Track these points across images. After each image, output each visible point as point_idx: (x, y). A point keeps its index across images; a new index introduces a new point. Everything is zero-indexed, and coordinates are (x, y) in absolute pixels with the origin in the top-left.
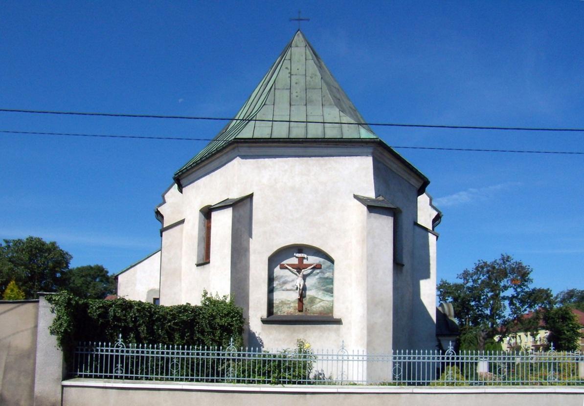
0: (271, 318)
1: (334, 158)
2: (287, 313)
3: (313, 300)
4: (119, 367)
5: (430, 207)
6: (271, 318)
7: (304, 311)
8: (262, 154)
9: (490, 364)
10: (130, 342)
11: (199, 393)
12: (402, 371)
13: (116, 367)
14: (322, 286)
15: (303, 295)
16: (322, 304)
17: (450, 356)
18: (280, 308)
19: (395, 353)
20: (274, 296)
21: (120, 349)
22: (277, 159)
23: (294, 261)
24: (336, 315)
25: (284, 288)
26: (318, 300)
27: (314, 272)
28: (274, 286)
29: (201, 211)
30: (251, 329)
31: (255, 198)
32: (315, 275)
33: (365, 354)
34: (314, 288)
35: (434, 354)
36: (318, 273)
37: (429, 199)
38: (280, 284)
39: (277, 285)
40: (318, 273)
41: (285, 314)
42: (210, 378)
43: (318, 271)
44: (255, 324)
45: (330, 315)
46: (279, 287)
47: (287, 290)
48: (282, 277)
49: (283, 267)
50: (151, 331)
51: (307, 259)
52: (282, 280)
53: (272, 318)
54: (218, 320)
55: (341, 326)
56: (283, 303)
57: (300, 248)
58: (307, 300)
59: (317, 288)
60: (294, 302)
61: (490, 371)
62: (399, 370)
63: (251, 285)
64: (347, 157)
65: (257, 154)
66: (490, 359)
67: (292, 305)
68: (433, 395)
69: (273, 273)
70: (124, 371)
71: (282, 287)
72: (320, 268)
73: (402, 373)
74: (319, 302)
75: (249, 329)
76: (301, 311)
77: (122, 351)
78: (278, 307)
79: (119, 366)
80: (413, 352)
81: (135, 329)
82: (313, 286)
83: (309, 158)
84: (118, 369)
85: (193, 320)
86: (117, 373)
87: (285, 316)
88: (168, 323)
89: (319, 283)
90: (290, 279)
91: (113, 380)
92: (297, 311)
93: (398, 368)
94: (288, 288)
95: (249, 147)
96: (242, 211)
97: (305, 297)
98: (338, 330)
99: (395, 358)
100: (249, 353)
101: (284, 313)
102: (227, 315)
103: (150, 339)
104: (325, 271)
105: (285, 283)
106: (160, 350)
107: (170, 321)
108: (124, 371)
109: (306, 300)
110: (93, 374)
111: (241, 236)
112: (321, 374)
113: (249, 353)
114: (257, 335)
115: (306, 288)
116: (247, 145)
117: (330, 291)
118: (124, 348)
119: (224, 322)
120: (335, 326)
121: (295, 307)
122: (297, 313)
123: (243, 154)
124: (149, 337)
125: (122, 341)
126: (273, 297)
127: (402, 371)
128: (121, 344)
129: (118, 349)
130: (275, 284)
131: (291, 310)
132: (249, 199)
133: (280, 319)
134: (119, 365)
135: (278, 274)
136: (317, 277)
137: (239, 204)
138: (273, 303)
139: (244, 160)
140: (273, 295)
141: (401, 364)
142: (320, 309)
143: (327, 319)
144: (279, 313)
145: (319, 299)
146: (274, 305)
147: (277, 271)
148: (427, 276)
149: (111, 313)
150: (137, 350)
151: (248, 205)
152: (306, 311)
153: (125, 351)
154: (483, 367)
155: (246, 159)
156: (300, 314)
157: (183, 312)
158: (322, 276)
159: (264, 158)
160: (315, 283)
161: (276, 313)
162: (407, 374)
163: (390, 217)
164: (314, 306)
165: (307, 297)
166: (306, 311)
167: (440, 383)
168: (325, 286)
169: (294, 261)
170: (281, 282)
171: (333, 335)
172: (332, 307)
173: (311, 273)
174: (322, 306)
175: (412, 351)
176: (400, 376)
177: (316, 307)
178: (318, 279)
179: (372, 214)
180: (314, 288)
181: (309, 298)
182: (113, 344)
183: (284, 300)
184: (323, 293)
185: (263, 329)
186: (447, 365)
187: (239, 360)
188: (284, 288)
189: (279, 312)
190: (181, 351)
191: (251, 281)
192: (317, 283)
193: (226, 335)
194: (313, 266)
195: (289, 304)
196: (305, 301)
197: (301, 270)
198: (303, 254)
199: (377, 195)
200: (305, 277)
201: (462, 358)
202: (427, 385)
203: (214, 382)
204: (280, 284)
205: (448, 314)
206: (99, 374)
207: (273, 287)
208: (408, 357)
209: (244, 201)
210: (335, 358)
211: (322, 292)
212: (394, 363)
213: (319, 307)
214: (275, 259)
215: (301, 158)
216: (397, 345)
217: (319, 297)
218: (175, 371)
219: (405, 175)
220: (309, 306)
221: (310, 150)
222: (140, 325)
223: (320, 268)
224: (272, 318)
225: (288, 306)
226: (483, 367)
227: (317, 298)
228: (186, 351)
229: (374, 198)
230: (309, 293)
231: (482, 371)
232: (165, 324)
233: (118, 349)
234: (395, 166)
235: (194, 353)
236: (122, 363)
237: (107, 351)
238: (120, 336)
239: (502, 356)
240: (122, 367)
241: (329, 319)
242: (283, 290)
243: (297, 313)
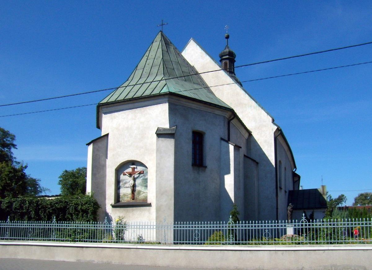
0: (118, 204)
1: (149, 107)
2: (127, 201)
3: (139, 192)
4: (231, 237)
5: (272, 124)
6: (118, 204)
7: (135, 199)
8: (108, 111)
9: (295, 229)
10: (25, 220)
11: (36, 247)
12: (200, 235)
13: (229, 237)
14: (144, 184)
15: (135, 190)
16: (144, 194)
17: (304, 224)
18: (123, 198)
19: (175, 224)
20: (120, 191)
21: (304, 224)
22: (121, 112)
23: (130, 170)
24: (149, 202)
25: (125, 186)
26: (142, 192)
27: (140, 176)
28: (121, 185)
29: (204, 133)
30: (107, 211)
31: (109, 136)
32: (141, 178)
33: (155, 224)
34: (140, 185)
35: (348, 221)
36: (142, 176)
37: (271, 119)
38: (123, 184)
39: (122, 185)
40: (142, 176)
41: (126, 202)
42: (90, 240)
43: (142, 175)
44: (109, 209)
45: (146, 201)
46: (122, 186)
47: (127, 187)
48: (124, 180)
49: (125, 175)
50: (37, 213)
51: (137, 168)
52: (124, 181)
53: (118, 204)
54: (80, 207)
55: (151, 207)
56: (124, 195)
57: (133, 163)
58: (137, 192)
59: (141, 185)
60: (130, 194)
61: (295, 233)
62: (198, 235)
63: (107, 186)
64: (155, 105)
65: (110, 111)
66: (295, 226)
67: (129, 196)
68: (149, 250)
69: (120, 178)
70: (308, 239)
71: (124, 186)
72: (143, 173)
73: (200, 236)
74: (143, 193)
75: (106, 211)
76: (133, 199)
77: (232, 227)
78: (122, 197)
79: (231, 236)
80: (192, 223)
81: (28, 213)
82: (140, 184)
83: (136, 109)
84: (230, 239)
85: (65, 207)
86: (230, 241)
87: (126, 202)
88: (48, 209)
89: (142, 182)
90: (128, 181)
91: (191, 245)
92: (131, 199)
93: (342, 236)
94: (127, 186)
95: (107, 107)
96: (100, 144)
97: (135, 191)
98: (149, 210)
99: (175, 227)
100: (207, 225)
101: (125, 201)
102: (86, 203)
103: (37, 218)
104: (145, 175)
105: (126, 183)
106: (257, 224)
107: (49, 208)
108: (234, 240)
109: (136, 193)
110: (179, 242)
111: (99, 158)
112: (141, 237)
113: (207, 225)
114: (109, 215)
115: (136, 185)
116: (105, 106)
117: (146, 186)
118: (233, 224)
119: (84, 207)
120: (148, 208)
121: (130, 197)
122: (132, 201)
123: (105, 112)
124: (36, 217)
125: (55, 220)
126: (120, 192)
127: (200, 235)
128: (232, 222)
129: (303, 224)
130: (121, 184)
131: (129, 199)
132: (106, 137)
133: (123, 204)
134: (231, 236)
135: (122, 179)
136: (141, 179)
137: (98, 141)
138: (120, 196)
139: (105, 115)
140: (120, 191)
141: (199, 231)
142: (143, 198)
143: (145, 204)
144: (123, 201)
145: (143, 192)
146: (120, 197)
147: (122, 177)
148: (229, 172)
149: (14, 206)
150: (198, 225)
151: (106, 139)
152: (136, 199)
153: (308, 225)
154: (290, 231)
155: (106, 114)
156: (133, 201)
157: (59, 203)
158: (144, 178)
159: (115, 113)
160: (141, 183)
161: (122, 201)
162: (180, 238)
163: (173, 139)
164: (140, 196)
165: (137, 191)
166: (136, 199)
167: (251, 243)
168: (145, 184)
169: (130, 170)
170: (124, 183)
171: (147, 214)
172: (147, 197)
173: (139, 176)
174: (144, 196)
175: (209, 222)
176: (199, 239)
177: (141, 197)
178: (142, 180)
179: (160, 138)
180: (140, 185)
181: (138, 191)
182: (51, 222)
183: (125, 193)
184: (144, 188)
185: (112, 211)
186: (219, 231)
187: (220, 230)
188: (125, 186)
189: (123, 201)
190: (244, 225)
191: (107, 183)
192: (142, 183)
193: (85, 215)
194: (138, 172)
195: (128, 195)
196: (136, 193)
197: (132, 175)
198: (134, 166)
199: (171, 126)
200: (135, 179)
201: (228, 226)
202: (203, 244)
203: (202, 244)
204: (123, 184)
205: (322, 193)
206: (182, 242)
207: (120, 186)
208: (186, 227)
209: (102, 139)
210: (149, 227)
211: (144, 187)
212: (174, 230)
213: (143, 197)
214: (120, 170)
215: (132, 110)
216: (178, 218)
217: (143, 190)
218: (197, 238)
219: (209, 110)
220: (137, 196)
221: (137, 104)
222: (31, 211)
223: (143, 173)
224: (118, 204)
225: (127, 197)
226: (290, 231)
227: (141, 191)
228: (253, 225)
229: (169, 128)
230: (138, 189)
231: (289, 234)
232: (46, 210)
233: (303, 224)
234: (194, 105)
235: (345, 224)
236: (232, 234)
237: (180, 227)
238: (55, 217)
239: (300, 224)
240: (233, 237)
241: (145, 204)
242: (125, 188)
243: (132, 201)
